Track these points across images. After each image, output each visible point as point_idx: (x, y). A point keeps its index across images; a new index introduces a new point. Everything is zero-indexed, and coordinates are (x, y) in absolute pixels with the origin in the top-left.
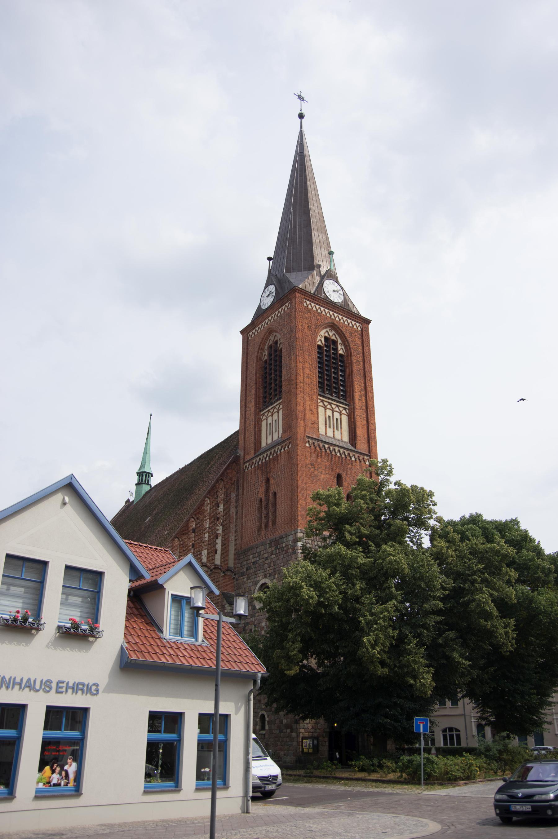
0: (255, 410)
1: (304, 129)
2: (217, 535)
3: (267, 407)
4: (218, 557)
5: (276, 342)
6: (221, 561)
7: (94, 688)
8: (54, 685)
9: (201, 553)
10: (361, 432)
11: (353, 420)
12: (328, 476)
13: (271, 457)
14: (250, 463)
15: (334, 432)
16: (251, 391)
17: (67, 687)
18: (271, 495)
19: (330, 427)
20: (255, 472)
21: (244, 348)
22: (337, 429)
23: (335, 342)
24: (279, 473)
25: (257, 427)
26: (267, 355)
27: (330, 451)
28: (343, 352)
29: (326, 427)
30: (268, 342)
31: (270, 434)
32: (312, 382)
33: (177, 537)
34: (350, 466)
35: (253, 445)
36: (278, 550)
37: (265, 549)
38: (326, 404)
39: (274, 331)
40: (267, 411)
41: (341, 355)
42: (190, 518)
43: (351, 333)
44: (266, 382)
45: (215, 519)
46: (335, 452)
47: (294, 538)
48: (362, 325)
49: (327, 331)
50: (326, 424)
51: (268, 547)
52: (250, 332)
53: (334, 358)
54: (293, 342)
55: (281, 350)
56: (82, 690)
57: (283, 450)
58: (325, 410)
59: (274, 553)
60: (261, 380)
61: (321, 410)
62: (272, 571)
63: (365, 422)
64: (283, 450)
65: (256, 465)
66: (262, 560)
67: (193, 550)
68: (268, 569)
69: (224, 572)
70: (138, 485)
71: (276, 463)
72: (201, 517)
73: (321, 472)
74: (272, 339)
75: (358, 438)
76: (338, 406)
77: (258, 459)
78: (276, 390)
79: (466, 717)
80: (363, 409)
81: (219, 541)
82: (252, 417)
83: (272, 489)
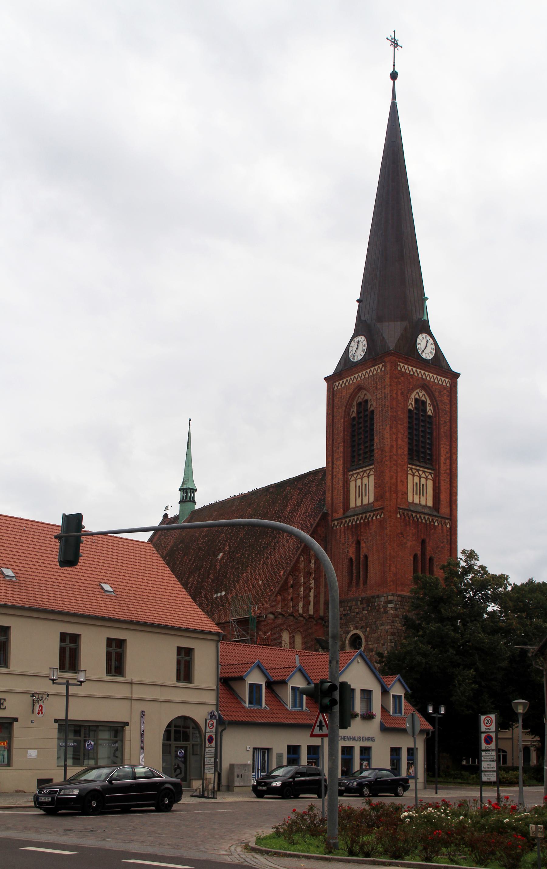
0: (344, 470)
1: (398, 100)
2: (310, 589)
3: (356, 469)
4: (311, 607)
5: (366, 401)
6: (314, 612)
7: (373, 739)
8: (361, 738)
9: (298, 606)
10: (444, 497)
11: (437, 485)
12: (414, 542)
13: (362, 521)
14: (339, 521)
15: (420, 498)
16: (338, 448)
17: (365, 739)
18: (362, 556)
19: (416, 494)
20: (344, 532)
21: (330, 399)
22: (423, 495)
23: (424, 403)
24: (371, 538)
25: (345, 487)
26: (355, 412)
27: (417, 518)
28: (431, 412)
29: (413, 494)
30: (357, 398)
31: (359, 496)
32: (403, 452)
33: (279, 593)
34: (433, 531)
35: (341, 505)
36: (369, 608)
37: (356, 604)
38: (414, 471)
39: (364, 389)
40: (356, 473)
41: (429, 416)
42: (289, 575)
43: (440, 392)
44: (354, 441)
45: (308, 574)
46: (421, 519)
47: (386, 600)
48: (451, 380)
49: (417, 393)
50: (413, 492)
51: (359, 603)
52: (336, 382)
53: (422, 421)
54: (387, 412)
55: (372, 412)
56: (370, 740)
57: (374, 518)
58: (413, 477)
59: (365, 609)
60: (349, 438)
61: (410, 477)
62: (364, 624)
63: (449, 486)
64: (374, 518)
65: (346, 525)
66: (353, 614)
67: (291, 603)
68: (360, 622)
69: (316, 621)
70: (181, 503)
71: (367, 528)
72: (297, 573)
73: (408, 540)
74: (362, 396)
75: (442, 503)
76: (424, 472)
77: (348, 520)
78: (365, 453)
79: (514, 740)
80: (447, 473)
81: (312, 594)
82: (340, 476)
83: (363, 552)
